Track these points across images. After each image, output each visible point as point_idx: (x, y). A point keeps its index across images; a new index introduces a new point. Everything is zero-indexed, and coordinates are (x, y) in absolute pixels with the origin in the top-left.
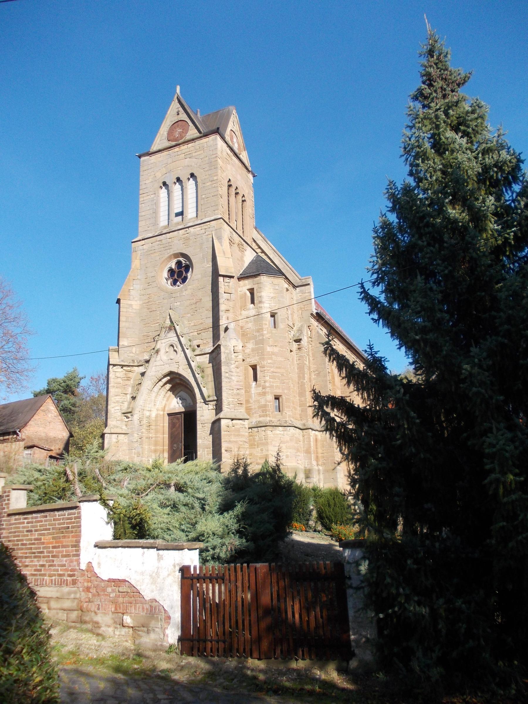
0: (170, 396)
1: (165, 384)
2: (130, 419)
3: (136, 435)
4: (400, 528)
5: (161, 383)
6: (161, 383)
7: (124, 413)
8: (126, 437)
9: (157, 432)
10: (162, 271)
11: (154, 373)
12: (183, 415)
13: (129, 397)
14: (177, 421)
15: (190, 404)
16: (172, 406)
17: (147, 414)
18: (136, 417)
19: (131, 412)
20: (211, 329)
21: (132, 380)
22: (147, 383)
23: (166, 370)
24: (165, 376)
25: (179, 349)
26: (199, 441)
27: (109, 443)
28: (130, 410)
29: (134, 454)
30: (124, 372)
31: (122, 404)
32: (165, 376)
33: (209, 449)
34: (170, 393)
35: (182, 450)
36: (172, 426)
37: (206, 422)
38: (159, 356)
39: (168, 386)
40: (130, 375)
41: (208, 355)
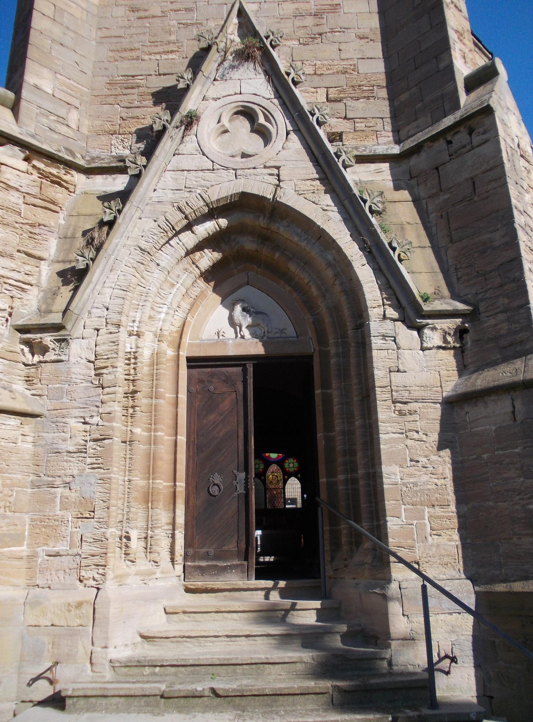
0: (202, 295)
1: (199, 247)
2: (50, 356)
3: (74, 424)
4: (267, 559)
5: (189, 239)
6: (189, 239)
7: (22, 330)
8: (26, 429)
9: (153, 423)
10: (24, 212)
11: (170, 196)
12: (250, 369)
13: (46, 273)
14: (224, 388)
15: (282, 331)
16: (208, 332)
17: (128, 344)
18: (79, 350)
19: (58, 328)
20: (384, 93)
21: (61, 215)
22: (136, 226)
23: (224, 187)
24: (213, 213)
25: (281, 122)
26: (392, 474)
27: (257, 595)
28: (56, 318)
29: (63, 508)
30: (36, 175)
31: (15, 292)
32: (213, 213)
33: (438, 511)
34: (206, 288)
35: (247, 496)
36: (201, 403)
37: (416, 394)
38: (191, 139)
39: (208, 258)
40: (57, 193)
41: (386, 166)
